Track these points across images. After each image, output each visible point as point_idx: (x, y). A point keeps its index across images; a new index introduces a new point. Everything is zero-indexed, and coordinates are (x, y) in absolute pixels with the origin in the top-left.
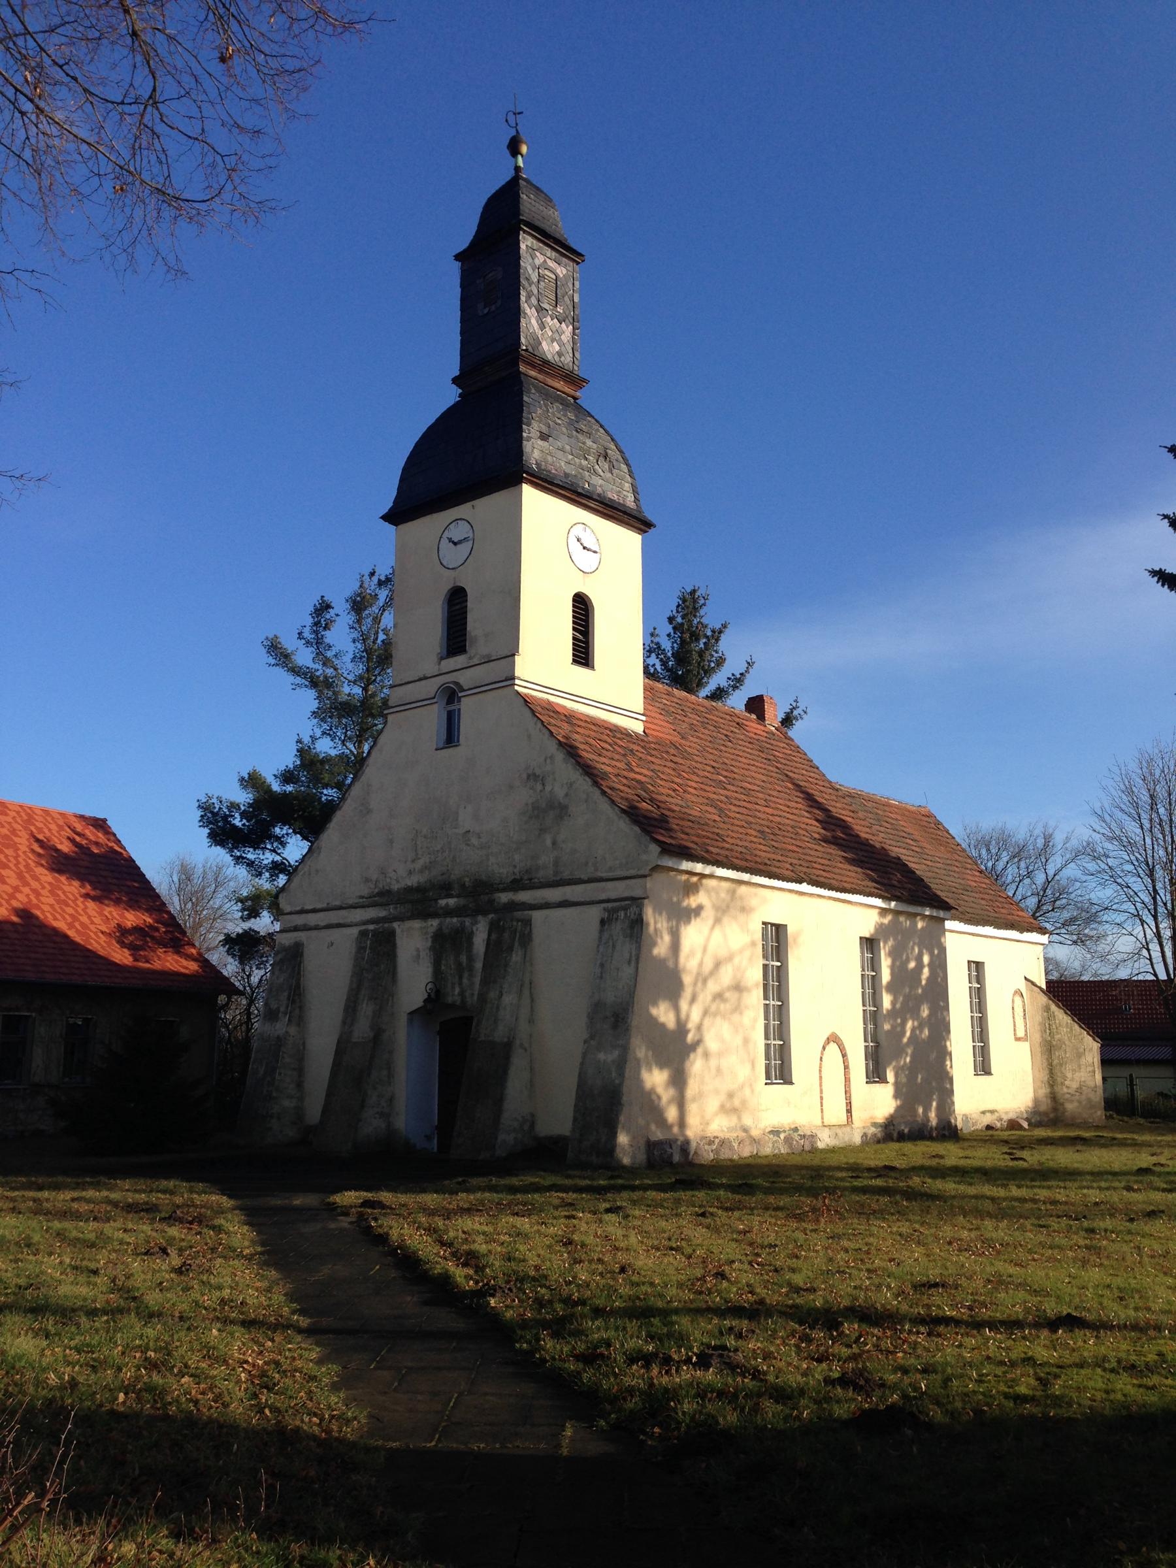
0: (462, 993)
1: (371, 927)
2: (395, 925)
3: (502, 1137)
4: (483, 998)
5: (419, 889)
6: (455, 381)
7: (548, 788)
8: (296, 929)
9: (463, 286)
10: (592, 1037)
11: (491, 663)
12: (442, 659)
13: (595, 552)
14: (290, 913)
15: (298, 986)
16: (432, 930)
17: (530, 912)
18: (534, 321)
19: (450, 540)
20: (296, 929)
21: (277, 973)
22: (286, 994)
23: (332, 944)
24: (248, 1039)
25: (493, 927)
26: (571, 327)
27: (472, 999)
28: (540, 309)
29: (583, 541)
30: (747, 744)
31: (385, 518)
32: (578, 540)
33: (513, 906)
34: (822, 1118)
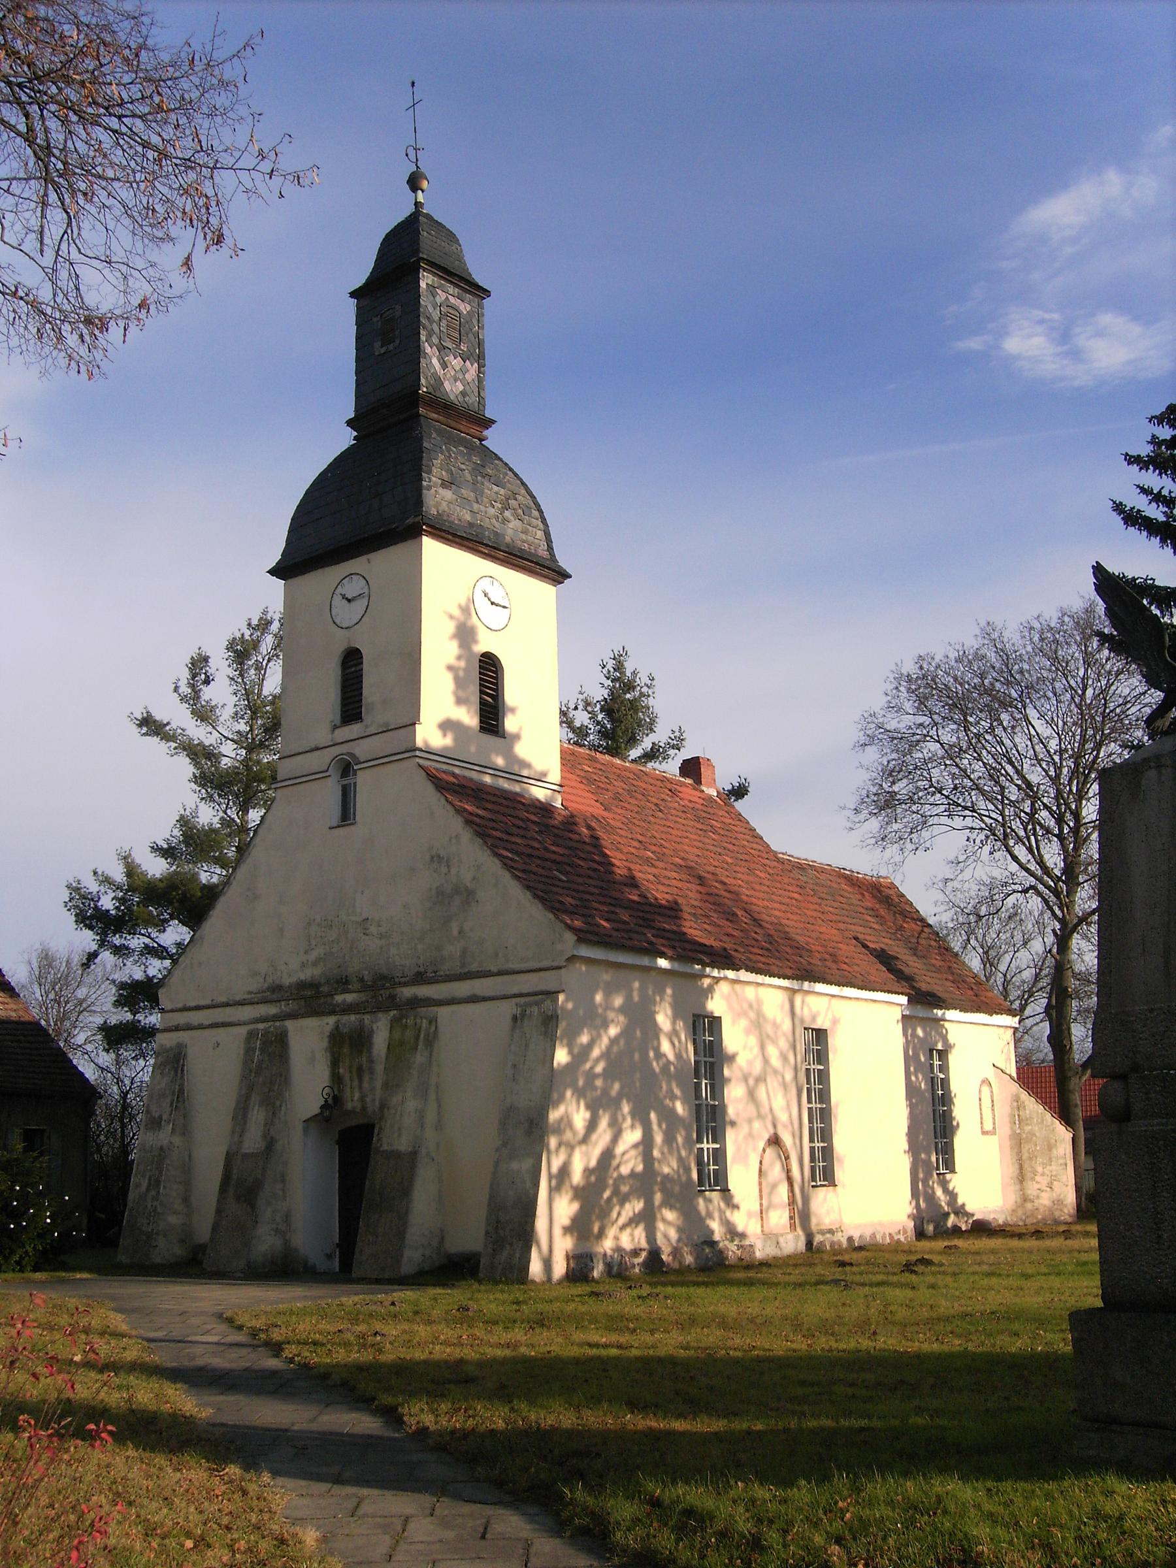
0: (362, 1099)
1: (261, 1026)
2: (289, 1024)
3: (407, 1253)
4: (383, 1106)
5: (313, 985)
6: (350, 423)
7: (454, 871)
8: (177, 1028)
9: (359, 323)
10: (505, 1144)
11: (390, 733)
12: (335, 727)
13: (504, 607)
14: (172, 1011)
15: (181, 1091)
16: (328, 1029)
17: (435, 1008)
18: (435, 361)
19: (344, 597)
20: (177, 1028)
21: (158, 1077)
22: (168, 1100)
23: (218, 1044)
24: (125, 1150)
25: (394, 1023)
26: (476, 365)
27: (373, 1106)
28: (442, 348)
29: (489, 595)
30: (680, 814)
31: (273, 572)
32: (486, 595)
33: (416, 1003)
34: (762, 1226)
